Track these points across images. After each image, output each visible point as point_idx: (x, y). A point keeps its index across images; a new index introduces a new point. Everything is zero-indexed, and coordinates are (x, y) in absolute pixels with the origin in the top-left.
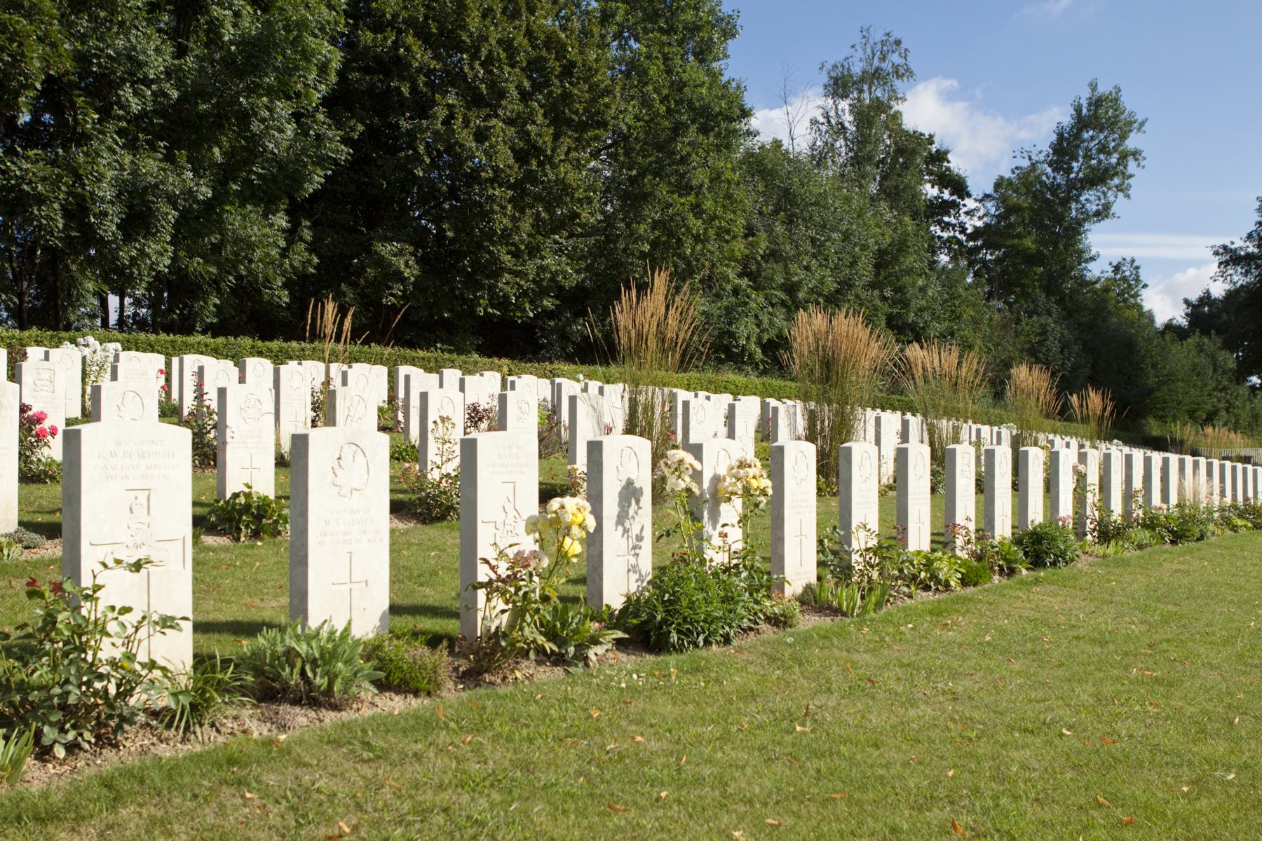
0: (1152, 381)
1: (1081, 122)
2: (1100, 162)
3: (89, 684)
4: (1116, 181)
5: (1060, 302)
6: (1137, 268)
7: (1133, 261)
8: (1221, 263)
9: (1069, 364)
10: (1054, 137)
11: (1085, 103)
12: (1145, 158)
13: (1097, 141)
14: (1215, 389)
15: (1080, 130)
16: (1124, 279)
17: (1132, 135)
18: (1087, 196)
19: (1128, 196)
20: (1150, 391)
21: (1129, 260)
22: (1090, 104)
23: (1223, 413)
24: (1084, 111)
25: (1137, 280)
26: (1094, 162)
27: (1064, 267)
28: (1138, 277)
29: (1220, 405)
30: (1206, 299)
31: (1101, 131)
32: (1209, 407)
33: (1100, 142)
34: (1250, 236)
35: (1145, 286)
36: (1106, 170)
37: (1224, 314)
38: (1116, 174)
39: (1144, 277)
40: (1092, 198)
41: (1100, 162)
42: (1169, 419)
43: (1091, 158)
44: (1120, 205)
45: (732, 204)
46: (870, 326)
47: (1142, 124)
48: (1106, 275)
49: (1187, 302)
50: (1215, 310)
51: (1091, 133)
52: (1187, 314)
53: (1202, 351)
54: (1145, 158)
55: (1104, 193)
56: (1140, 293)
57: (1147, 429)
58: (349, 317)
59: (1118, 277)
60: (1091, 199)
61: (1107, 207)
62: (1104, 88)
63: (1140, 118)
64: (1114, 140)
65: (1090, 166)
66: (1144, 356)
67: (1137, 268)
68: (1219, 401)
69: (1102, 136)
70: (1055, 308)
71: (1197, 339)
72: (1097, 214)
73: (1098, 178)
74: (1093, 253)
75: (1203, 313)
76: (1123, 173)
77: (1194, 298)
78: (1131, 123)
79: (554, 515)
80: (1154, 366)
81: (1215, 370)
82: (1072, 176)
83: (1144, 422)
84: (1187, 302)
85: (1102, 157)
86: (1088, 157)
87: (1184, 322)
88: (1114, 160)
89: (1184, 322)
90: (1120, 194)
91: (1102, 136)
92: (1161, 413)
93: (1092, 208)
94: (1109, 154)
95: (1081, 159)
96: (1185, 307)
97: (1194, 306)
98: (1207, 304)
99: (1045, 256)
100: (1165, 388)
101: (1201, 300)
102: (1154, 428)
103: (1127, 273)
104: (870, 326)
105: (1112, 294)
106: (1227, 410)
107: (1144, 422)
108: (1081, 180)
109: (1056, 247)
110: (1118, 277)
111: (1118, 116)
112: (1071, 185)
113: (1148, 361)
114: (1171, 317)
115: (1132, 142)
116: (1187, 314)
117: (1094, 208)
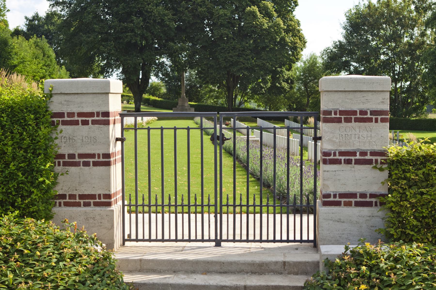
3: (396, 37)
8: (51, 5)
25: (4, 7)
28: (5, 6)
29: (47, 73)
30: (36, 17)
35: (8, 11)
37: (46, 26)
45: (401, 166)
49: (26, 18)
50: (41, 23)
52: (26, 24)
53: (37, 46)
56: (6, 14)
68: (46, 71)
75: (35, 24)
77: (30, 16)
80: (16, 54)
81: (44, 56)
84: (26, 18)
87: (25, 29)
89: (25, 29)
96: (25, 20)
97: (30, 20)
98: (36, 19)
100: (21, 65)
101: (34, 17)
114: (18, 25)
116: (26, 24)
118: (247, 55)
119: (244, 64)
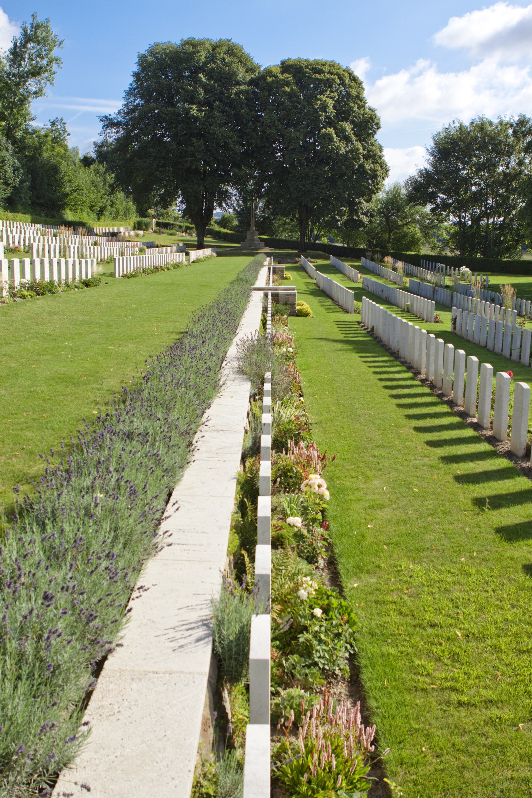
0: (68, 189)
1: (27, 38)
2: (37, 62)
4: (46, 75)
5: (14, 143)
6: (64, 124)
7: (62, 120)
8: (104, 126)
9: (18, 180)
10: (11, 45)
11: (29, 27)
12: (62, 63)
13: (35, 50)
14: (105, 194)
15: (26, 42)
16: (57, 130)
17: (55, 49)
18: (29, 82)
19: (52, 84)
20: (67, 195)
21: (59, 118)
22: (32, 27)
23: (109, 207)
24: (29, 31)
25: (65, 131)
26: (34, 62)
27: (17, 123)
31: (38, 44)
32: (101, 204)
33: (37, 50)
34: (119, 112)
35: (68, 135)
36: (41, 68)
38: (46, 71)
39: (68, 129)
40: (32, 83)
41: (37, 62)
42: (79, 211)
43: (32, 60)
44: (48, 90)
46: (359, 703)
47: (61, 43)
48: (47, 127)
51: (32, 44)
54: (62, 63)
55: (40, 82)
57: (65, 216)
58: (507, 259)
59: (54, 128)
60: (32, 84)
61: (41, 90)
62: (40, 19)
63: (60, 39)
64: (45, 51)
65: (31, 65)
66: (64, 175)
67: (64, 124)
68: (107, 201)
69: (38, 47)
70: (10, 147)
71: (96, 166)
72: (35, 93)
73: (36, 72)
74: (32, 116)
76: (50, 71)
78: (55, 41)
79: (63, 151)
80: (70, 181)
82: (21, 69)
83: (63, 212)
85: (38, 59)
86: (30, 59)
87: (93, 155)
88: (45, 62)
89: (93, 155)
90: (48, 83)
91: (38, 47)
92: (73, 208)
93: (33, 89)
94: (43, 58)
95: (26, 60)
97: (99, 146)
99: (6, 116)
102: (69, 215)
103: (59, 127)
104: (359, 703)
105: (49, 139)
106: (112, 206)
107: (63, 212)
108: (26, 73)
109: (12, 111)
110: (54, 128)
111: (48, 36)
112: (20, 76)
113: (66, 178)
115: (55, 52)
117: (34, 89)
118: (321, 184)
119: (317, 193)
